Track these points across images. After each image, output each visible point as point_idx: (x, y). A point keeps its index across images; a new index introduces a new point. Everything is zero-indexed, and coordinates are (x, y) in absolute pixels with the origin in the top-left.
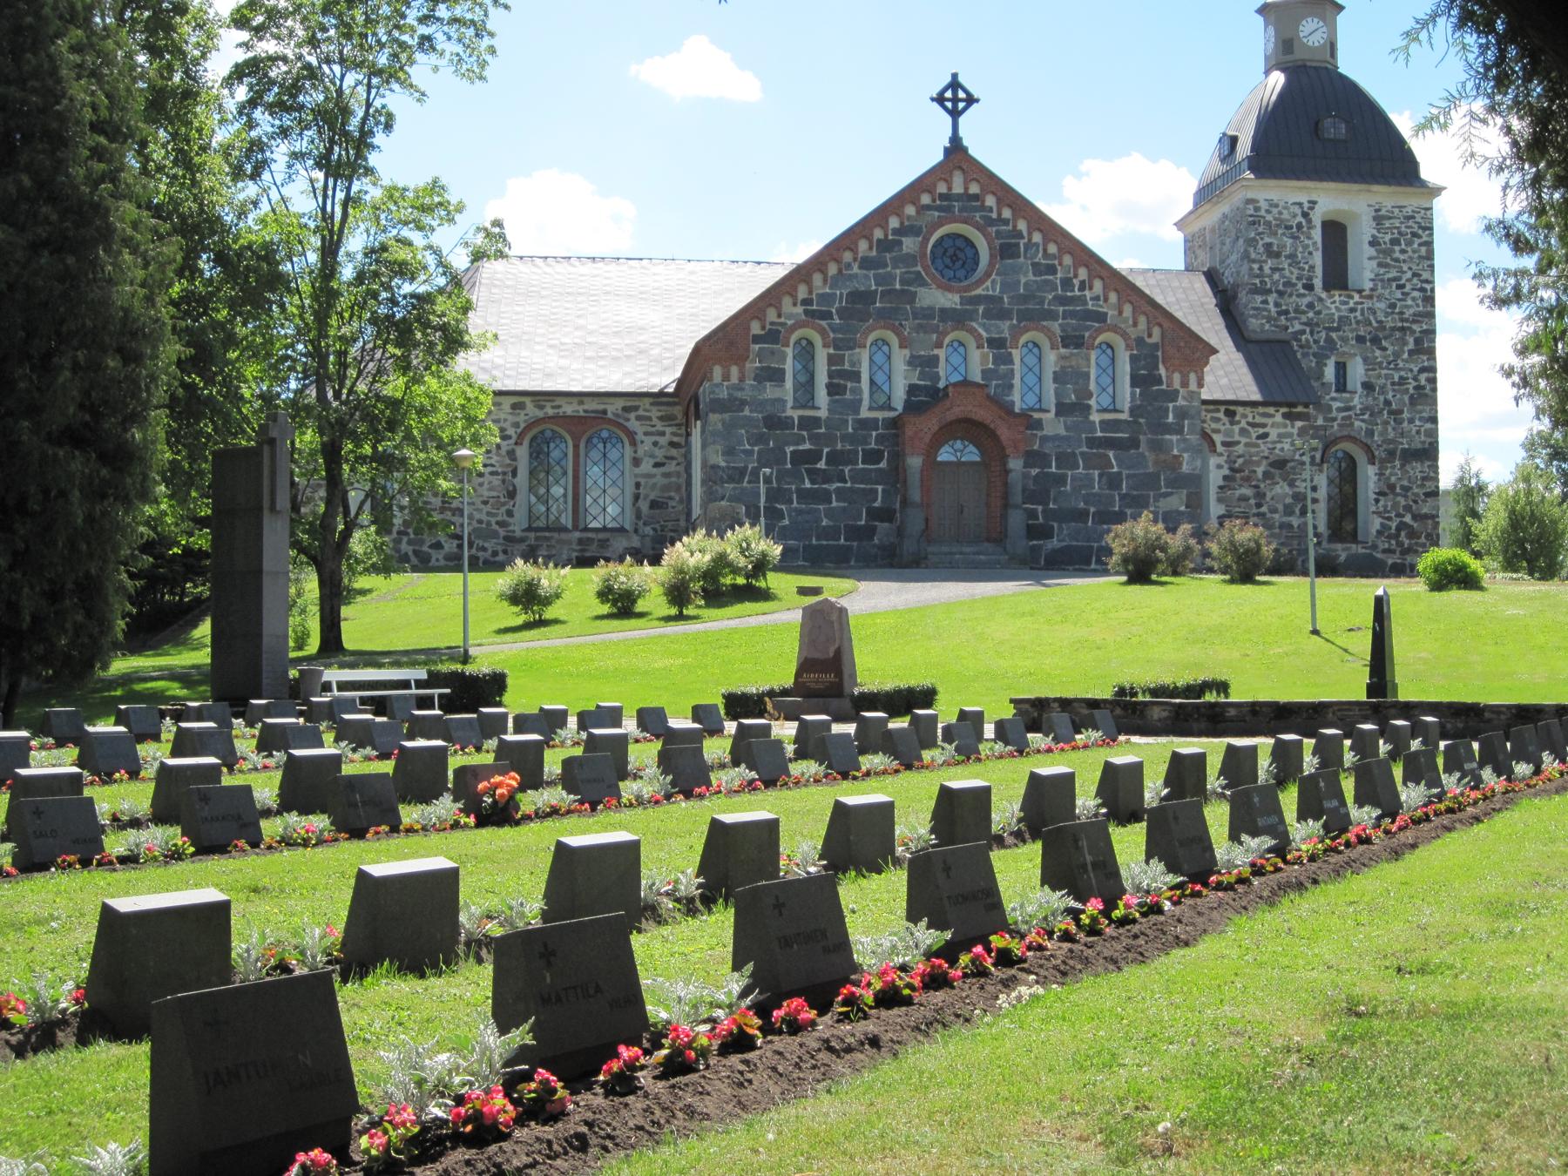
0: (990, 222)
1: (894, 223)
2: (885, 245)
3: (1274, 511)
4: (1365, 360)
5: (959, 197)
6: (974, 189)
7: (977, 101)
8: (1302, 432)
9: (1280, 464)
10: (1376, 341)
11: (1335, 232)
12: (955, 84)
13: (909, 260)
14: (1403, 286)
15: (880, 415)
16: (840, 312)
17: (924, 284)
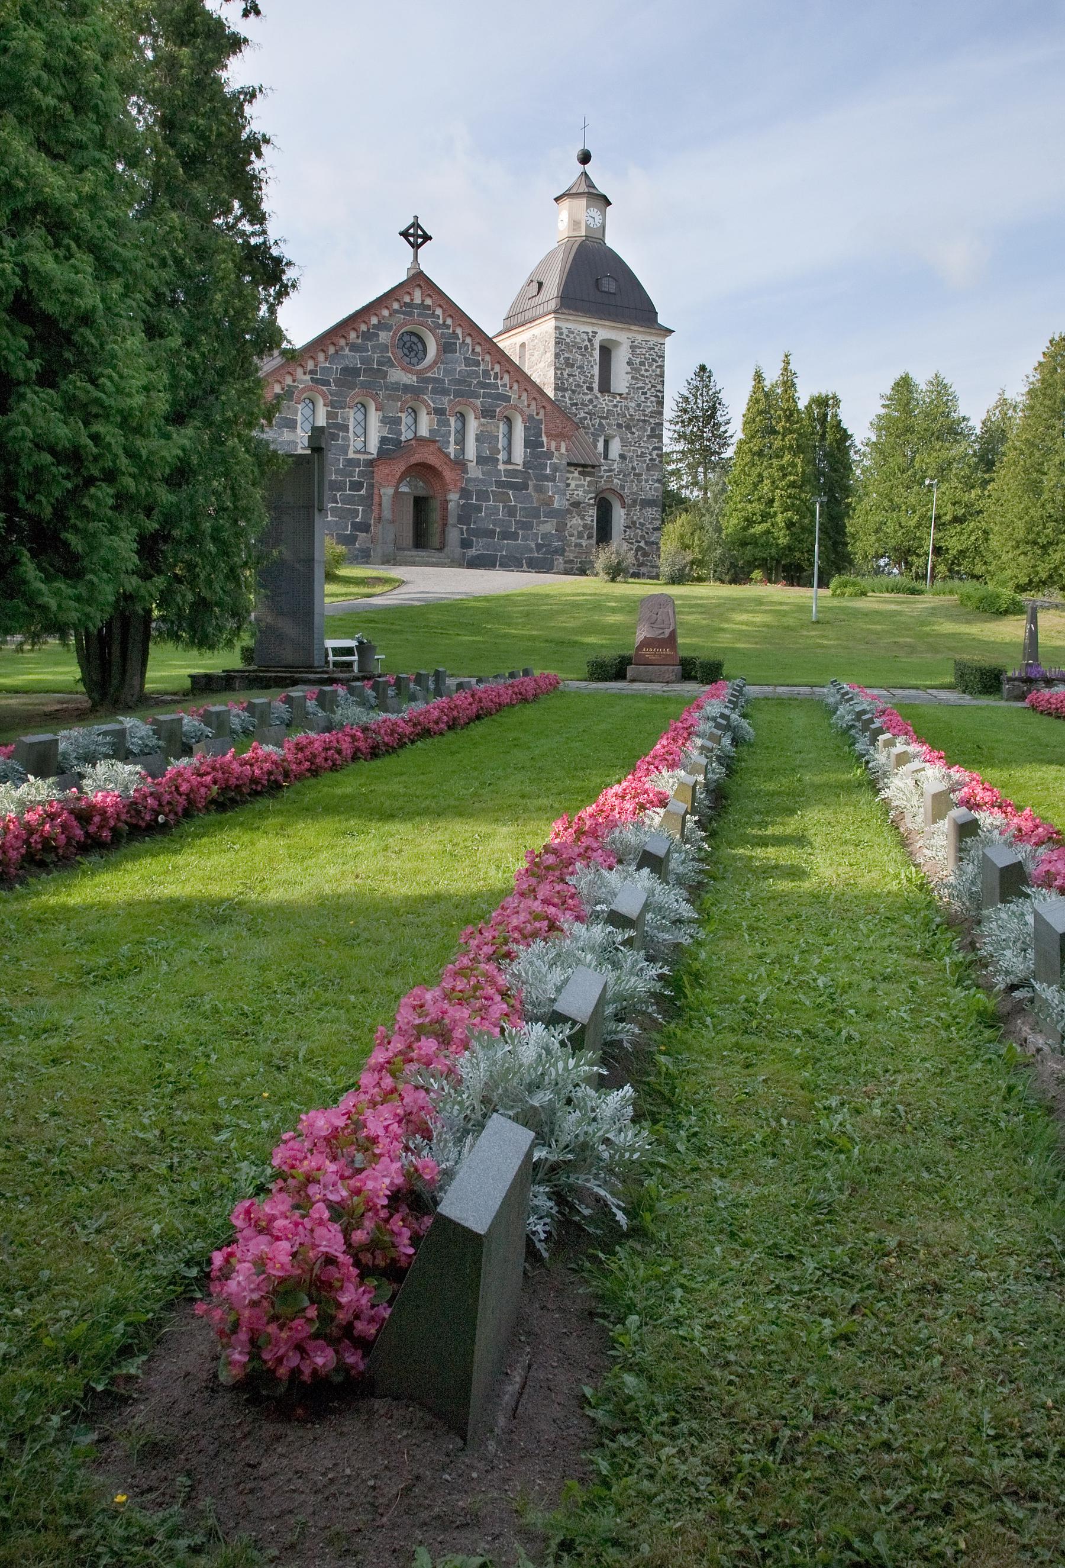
0: (438, 326)
1: (374, 320)
2: (367, 336)
3: (572, 535)
4: (622, 439)
5: (418, 306)
6: (428, 302)
7: (430, 238)
8: (590, 484)
9: (576, 504)
10: (628, 427)
11: (606, 351)
12: (416, 225)
13: (385, 348)
14: (644, 393)
15: (361, 457)
16: (337, 382)
17: (393, 366)
